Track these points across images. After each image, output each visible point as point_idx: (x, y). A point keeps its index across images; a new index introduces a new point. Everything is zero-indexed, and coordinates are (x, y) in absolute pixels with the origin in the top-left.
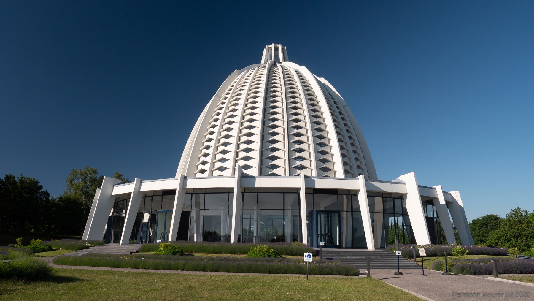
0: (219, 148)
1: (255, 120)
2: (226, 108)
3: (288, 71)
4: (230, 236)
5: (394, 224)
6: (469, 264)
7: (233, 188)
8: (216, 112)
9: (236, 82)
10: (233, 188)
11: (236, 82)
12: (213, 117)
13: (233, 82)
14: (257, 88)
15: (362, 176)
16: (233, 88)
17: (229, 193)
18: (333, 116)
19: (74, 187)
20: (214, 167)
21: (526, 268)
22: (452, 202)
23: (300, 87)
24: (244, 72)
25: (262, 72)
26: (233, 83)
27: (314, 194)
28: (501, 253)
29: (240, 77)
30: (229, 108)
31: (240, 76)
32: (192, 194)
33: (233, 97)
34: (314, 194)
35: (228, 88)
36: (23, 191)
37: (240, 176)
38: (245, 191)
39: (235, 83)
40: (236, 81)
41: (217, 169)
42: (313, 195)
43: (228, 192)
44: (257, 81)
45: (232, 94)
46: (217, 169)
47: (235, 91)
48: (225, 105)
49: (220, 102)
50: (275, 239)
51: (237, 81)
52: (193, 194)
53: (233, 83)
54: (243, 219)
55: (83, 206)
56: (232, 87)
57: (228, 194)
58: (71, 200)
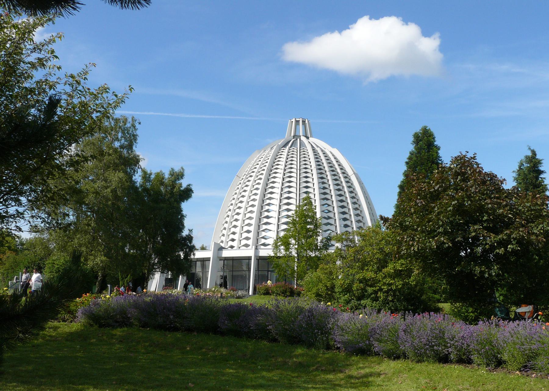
0: (249, 203)
1: (273, 198)
2: (253, 181)
6: (145, 302)
7: (251, 257)
10: (251, 257)
17: (249, 259)
18: (342, 170)
19: (394, 267)
20: (240, 244)
21: (183, 293)
23: (313, 164)
30: (257, 176)
32: (224, 260)
41: (245, 232)
45: (263, 161)
46: (245, 232)
47: (263, 163)
51: (264, 157)
52: (225, 261)
58: (451, 245)
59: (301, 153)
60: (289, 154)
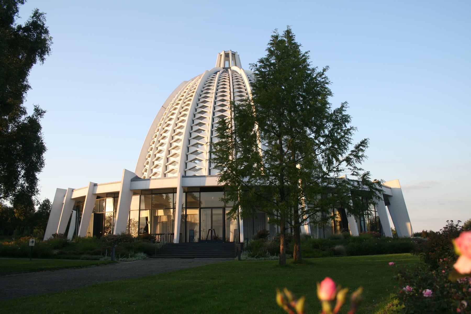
3: (238, 75)
4: (173, 234)
5: (368, 223)
7: (176, 188)
9: (186, 92)
10: (176, 188)
11: (186, 92)
12: (166, 123)
13: (182, 93)
16: (185, 94)
22: (392, 196)
24: (196, 79)
27: (201, 193)
29: (192, 84)
30: (180, 113)
31: (190, 85)
33: (185, 103)
34: (201, 193)
36: (463, 293)
37: (93, 185)
38: (189, 191)
39: (185, 92)
40: (186, 91)
42: (200, 193)
43: (173, 192)
49: (173, 108)
51: (187, 91)
54: (141, 212)
57: (173, 194)
59: (234, 81)
60: (219, 81)
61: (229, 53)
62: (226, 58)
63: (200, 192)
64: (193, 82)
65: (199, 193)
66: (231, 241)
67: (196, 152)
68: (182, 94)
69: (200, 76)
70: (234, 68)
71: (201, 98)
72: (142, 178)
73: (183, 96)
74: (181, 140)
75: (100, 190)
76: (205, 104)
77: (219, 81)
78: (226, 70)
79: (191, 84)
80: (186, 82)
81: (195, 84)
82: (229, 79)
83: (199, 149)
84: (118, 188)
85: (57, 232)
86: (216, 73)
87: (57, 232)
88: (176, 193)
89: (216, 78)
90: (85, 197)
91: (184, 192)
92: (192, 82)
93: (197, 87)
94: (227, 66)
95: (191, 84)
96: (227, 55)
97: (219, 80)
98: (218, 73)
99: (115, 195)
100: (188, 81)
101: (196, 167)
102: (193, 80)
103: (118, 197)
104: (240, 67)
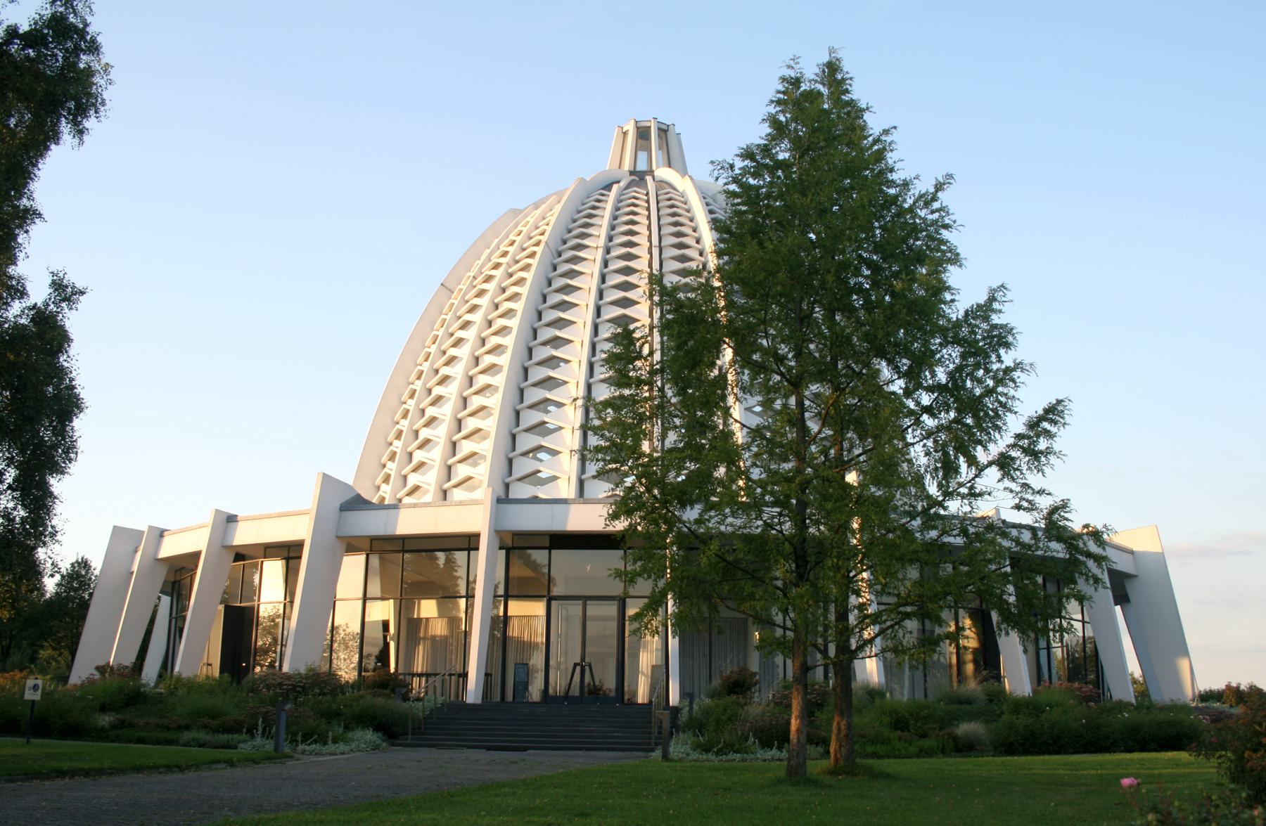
8: (468, 304)
9: (514, 241)
11: (514, 241)
14: (580, 247)
15: (232, 542)
16: (511, 249)
25: (599, 201)
26: (496, 258)
27: (553, 552)
28: (54, 475)
31: (528, 222)
33: (511, 275)
35: (492, 262)
40: (514, 238)
42: (550, 553)
43: (467, 547)
44: (585, 217)
45: (509, 266)
48: (502, 269)
50: (44, 393)
51: (518, 239)
53: (496, 258)
55: (816, 459)
56: (502, 256)
57: (466, 552)
60: (620, 205)
61: (650, 127)
62: (640, 141)
63: (550, 548)
64: (538, 212)
65: (547, 551)
66: (640, 701)
67: (540, 428)
68: (503, 248)
69: (559, 195)
70: (664, 173)
71: (559, 263)
72: (374, 501)
73: (505, 254)
74: (496, 389)
75: (244, 536)
76: (550, 390)
77: (619, 203)
78: (639, 177)
79: (531, 219)
80: (516, 212)
81: (544, 219)
82: (646, 205)
83: (552, 420)
84: (300, 529)
85: (112, 660)
86: (608, 187)
87: (112, 660)
88: (477, 549)
89: (605, 209)
90: (197, 555)
91: (501, 548)
92: (536, 212)
93: (549, 229)
94: (642, 166)
95: (531, 219)
96: (643, 134)
97: (618, 209)
98: (615, 187)
99: (289, 552)
100: (524, 207)
101: (539, 471)
102: (536, 206)
103: (300, 557)
104: (684, 172)
